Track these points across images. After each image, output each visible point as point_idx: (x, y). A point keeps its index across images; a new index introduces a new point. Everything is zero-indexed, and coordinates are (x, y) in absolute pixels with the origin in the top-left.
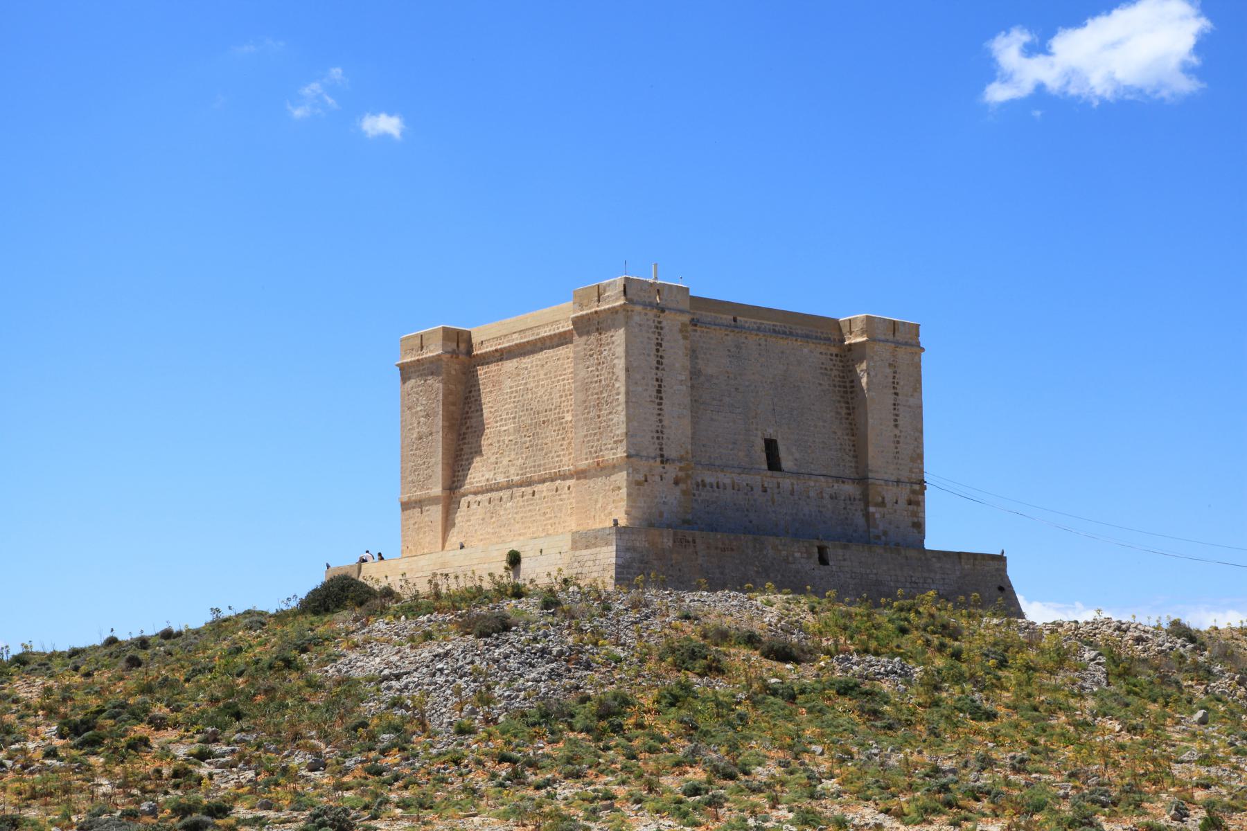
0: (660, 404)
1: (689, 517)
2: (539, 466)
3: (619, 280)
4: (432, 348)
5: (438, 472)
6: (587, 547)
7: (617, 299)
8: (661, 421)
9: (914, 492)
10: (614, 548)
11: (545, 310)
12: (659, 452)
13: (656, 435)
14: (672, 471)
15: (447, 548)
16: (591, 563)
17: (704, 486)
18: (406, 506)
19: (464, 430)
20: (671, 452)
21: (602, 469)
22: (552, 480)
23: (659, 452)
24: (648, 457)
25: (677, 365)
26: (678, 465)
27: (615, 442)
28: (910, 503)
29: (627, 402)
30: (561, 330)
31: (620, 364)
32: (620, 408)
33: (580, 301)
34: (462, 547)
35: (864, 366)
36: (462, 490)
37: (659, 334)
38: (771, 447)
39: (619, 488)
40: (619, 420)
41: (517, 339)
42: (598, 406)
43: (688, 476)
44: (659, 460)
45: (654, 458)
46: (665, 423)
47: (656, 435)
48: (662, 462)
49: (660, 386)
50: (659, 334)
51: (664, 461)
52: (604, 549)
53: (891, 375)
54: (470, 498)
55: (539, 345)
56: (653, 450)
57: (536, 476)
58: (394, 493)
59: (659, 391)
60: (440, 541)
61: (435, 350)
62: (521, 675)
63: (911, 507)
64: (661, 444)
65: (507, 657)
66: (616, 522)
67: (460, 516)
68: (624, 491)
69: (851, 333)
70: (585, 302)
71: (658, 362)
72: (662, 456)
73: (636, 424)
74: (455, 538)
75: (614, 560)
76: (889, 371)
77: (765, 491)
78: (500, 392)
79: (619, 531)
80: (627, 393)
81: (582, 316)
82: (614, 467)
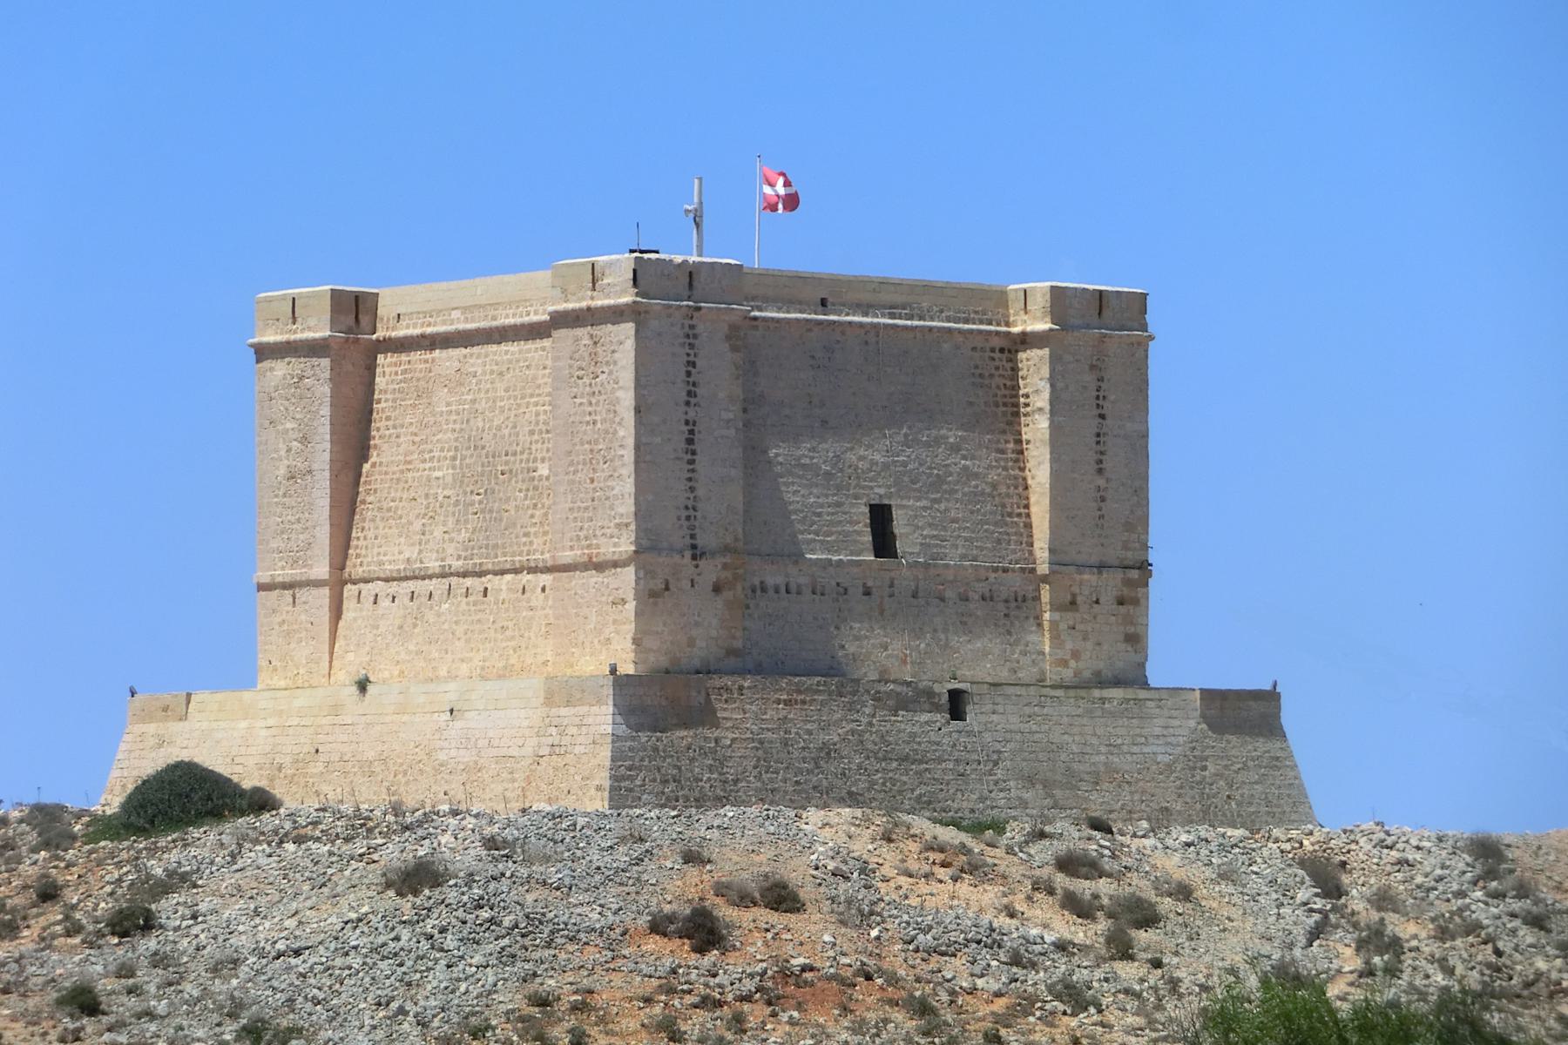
0: (691, 462)
1: (738, 644)
2: (496, 546)
4: (312, 322)
6: (568, 704)
8: (692, 489)
9: (1128, 583)
10: (611, 709)
12: (688, 541)
13: (684, 513)
14: (711, 570)
16: (574, 730)
17: (764, 590)
20: (705, 540)
22: (516, 571)
23: (688, 541)
24: (671, 549)
25: (721, 395)
26: (720, 560)
27: (618, 526)
28: (1121, 602)
29: (637, 462)
31: (627, 398)
37: (691, 346)
38: (880, 517)
39: (624, 601)
43: (736, 577)
44: (688, 554)
45: (681, 552)
46: (700, 492)
47: (684, 513)
48: (694, 557)
49: (691, 432)
50: (691, 346)
51: (697, 554)
52: (595, 709)
53: (1093, 386)
56: (679, 538)
59: (690, 441)
60: (326, 647)
62: (462, 957)
63: (1122, 609)
64: (692, 528)
65: (443, 930)
66: (613, 671)
68: (631, 606)
70: (572, 288)
71: (689, 393)
72: (694, 547)
73: (650, 498)
75: (609, 730)
76: (1089, 378)
77: (867, 593)
79: (621, 683)
80: (637, 447)
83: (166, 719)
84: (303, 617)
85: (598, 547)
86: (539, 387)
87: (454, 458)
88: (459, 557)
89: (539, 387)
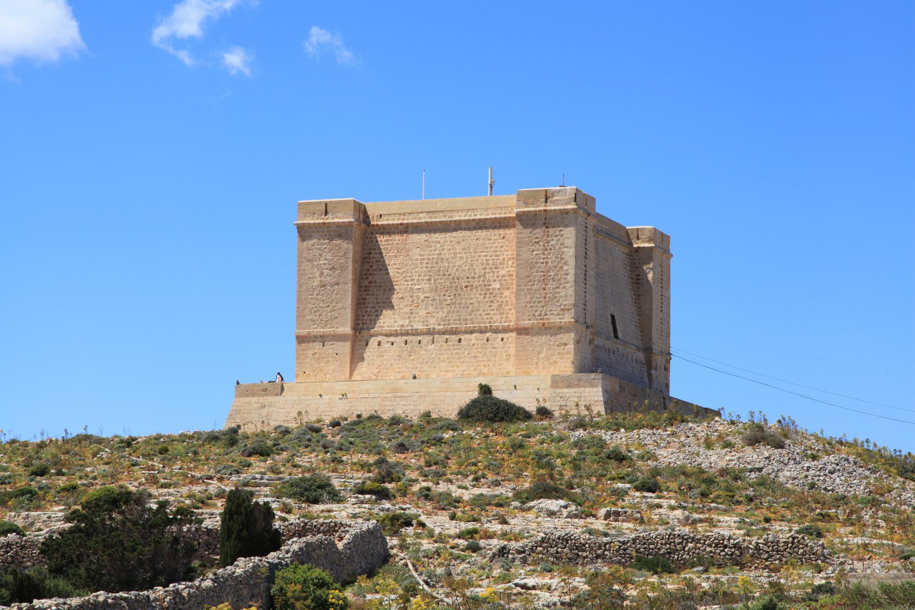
3: (570, 189)
5: (348, 314)
6: (568, 387)
7: (568, 203)
10: (600, 389)
11: (457, 199)
15: (356, 376)
18: (301, 340)
19: (366, 283)
21: (546, 329)
30: (478, 217)
32: (568, 285)
33: (525, 198)
34: (415, 377)
35: (651, 265)
36: (372, 331)
40: (568, 293)
41: (424, 219)
42: (544, 281)
54: (380, 338)
55: (453, 225)
57: (463, 327)
58: (291, 330)
61: (346, 217)
67: (371, 351)
69: (638, 238)
74: (363, 369)
78: (403, 259)
81: (529, 212)
82: (560, 328)
83: (266, 395)
84: (330, 351)
85: (548, 319)
86: (487, 248)
87: (429, 280)
88: (439, 325)
89: (487, 248)
